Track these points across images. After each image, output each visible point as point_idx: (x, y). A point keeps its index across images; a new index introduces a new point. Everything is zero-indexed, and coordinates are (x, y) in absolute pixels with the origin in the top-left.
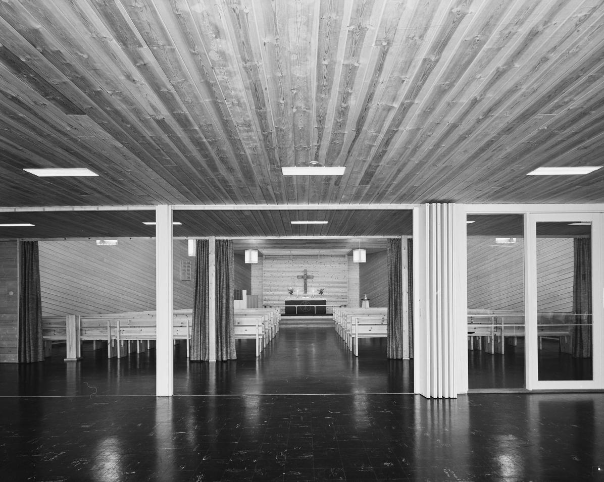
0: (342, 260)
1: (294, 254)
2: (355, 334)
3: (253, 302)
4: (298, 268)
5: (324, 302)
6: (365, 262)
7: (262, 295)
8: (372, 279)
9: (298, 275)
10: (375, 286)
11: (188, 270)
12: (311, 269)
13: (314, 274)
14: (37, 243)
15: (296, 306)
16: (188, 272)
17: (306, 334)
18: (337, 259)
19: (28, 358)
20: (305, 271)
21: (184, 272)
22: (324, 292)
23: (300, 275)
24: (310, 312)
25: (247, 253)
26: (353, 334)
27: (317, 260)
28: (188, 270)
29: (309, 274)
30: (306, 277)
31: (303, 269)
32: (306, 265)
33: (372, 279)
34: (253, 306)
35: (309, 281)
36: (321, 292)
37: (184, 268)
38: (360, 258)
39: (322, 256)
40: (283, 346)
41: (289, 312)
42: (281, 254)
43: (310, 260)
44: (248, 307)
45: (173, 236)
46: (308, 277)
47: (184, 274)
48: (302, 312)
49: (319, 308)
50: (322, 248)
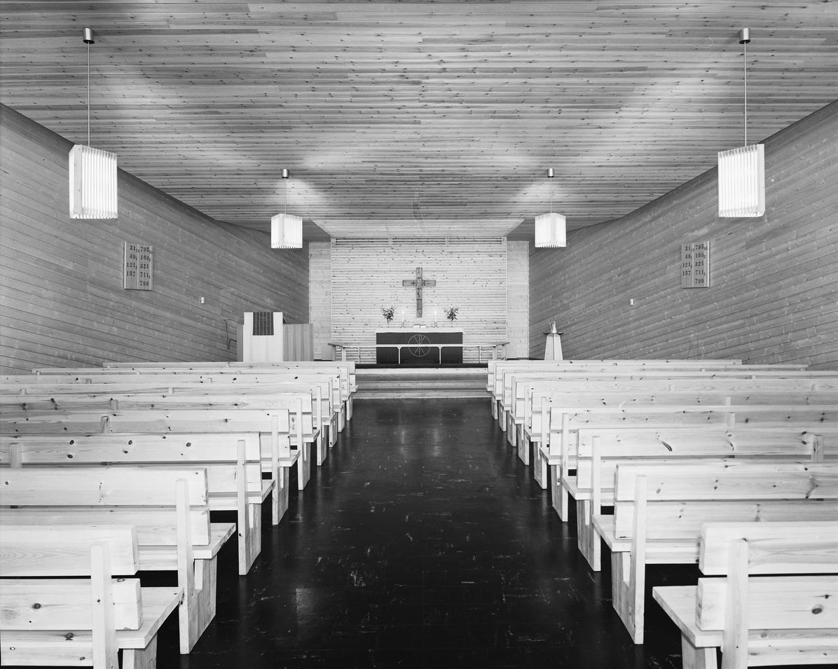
0: (496, 247)
1: (396, 235)
2: (540, 435)
4: (403, 263)
5: (458, 337)
6: (564, 245)
7: (329, 320)
8: (558, 288)
9: (404, 278)
10: (565, 302)
11: (144, 266)
12: (432, 266)
13: (438, 278)
15: (399, 346)
16: (143, 270)
17: (420, 413)
18: (484, 247)
19: (749, 157)
20: (419, 270)
22: (458, 315)
23: (408, 278)
24: (429, 359)
25: (276, 223)
26: (508, 406)
27: (444, 247)
28: (144, 266)
29: (426, 276)
30: (420, 284)
31: (414, 267)
32: (421, 257)
33: (558, 288)
34: (299, 356)
35: (426, 291)
36: (452, 316)
37: (132, 260)
38: (554, 235)
39: (454, 240)
40: (371, 432)
41: (385, 359)
42: (370, 235)
43: (428, 248)
46: (424, 283)
47: (131, 274)
48: (410, 360)
49: (443, 352)
50: (456, 217)
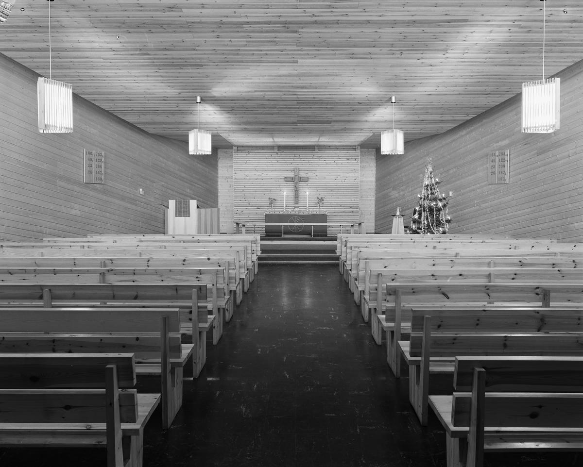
0: (352, 153)
3: (209, 223)
5: (323, 218)
13: (310, 174)
14: (376, 226)
16: (501, 176)
21: (492, 265)
25: (192, 137)
30: (296, 180)
44: (199, 231)
45: (135, 422)
46: (301, 179)
